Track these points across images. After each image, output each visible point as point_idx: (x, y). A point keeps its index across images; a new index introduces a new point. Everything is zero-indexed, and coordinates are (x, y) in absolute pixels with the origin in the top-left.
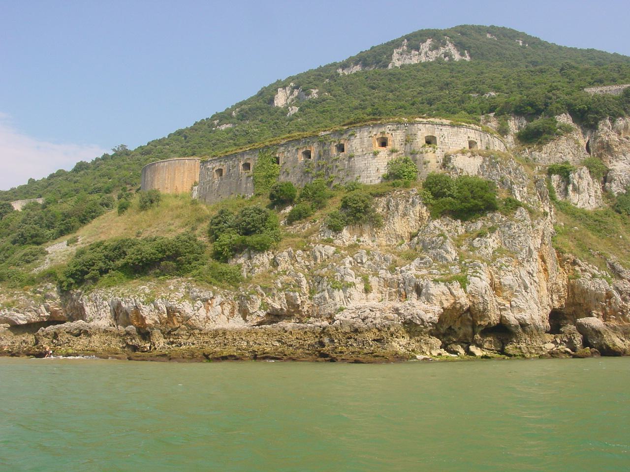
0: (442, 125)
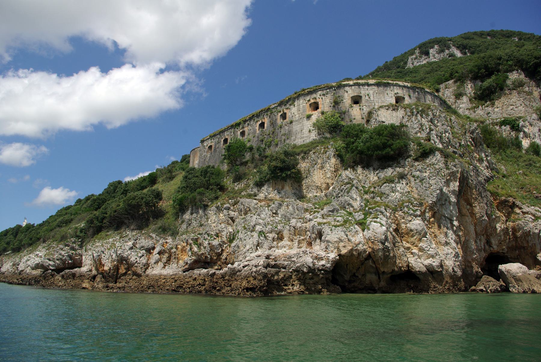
0: (368, 85)
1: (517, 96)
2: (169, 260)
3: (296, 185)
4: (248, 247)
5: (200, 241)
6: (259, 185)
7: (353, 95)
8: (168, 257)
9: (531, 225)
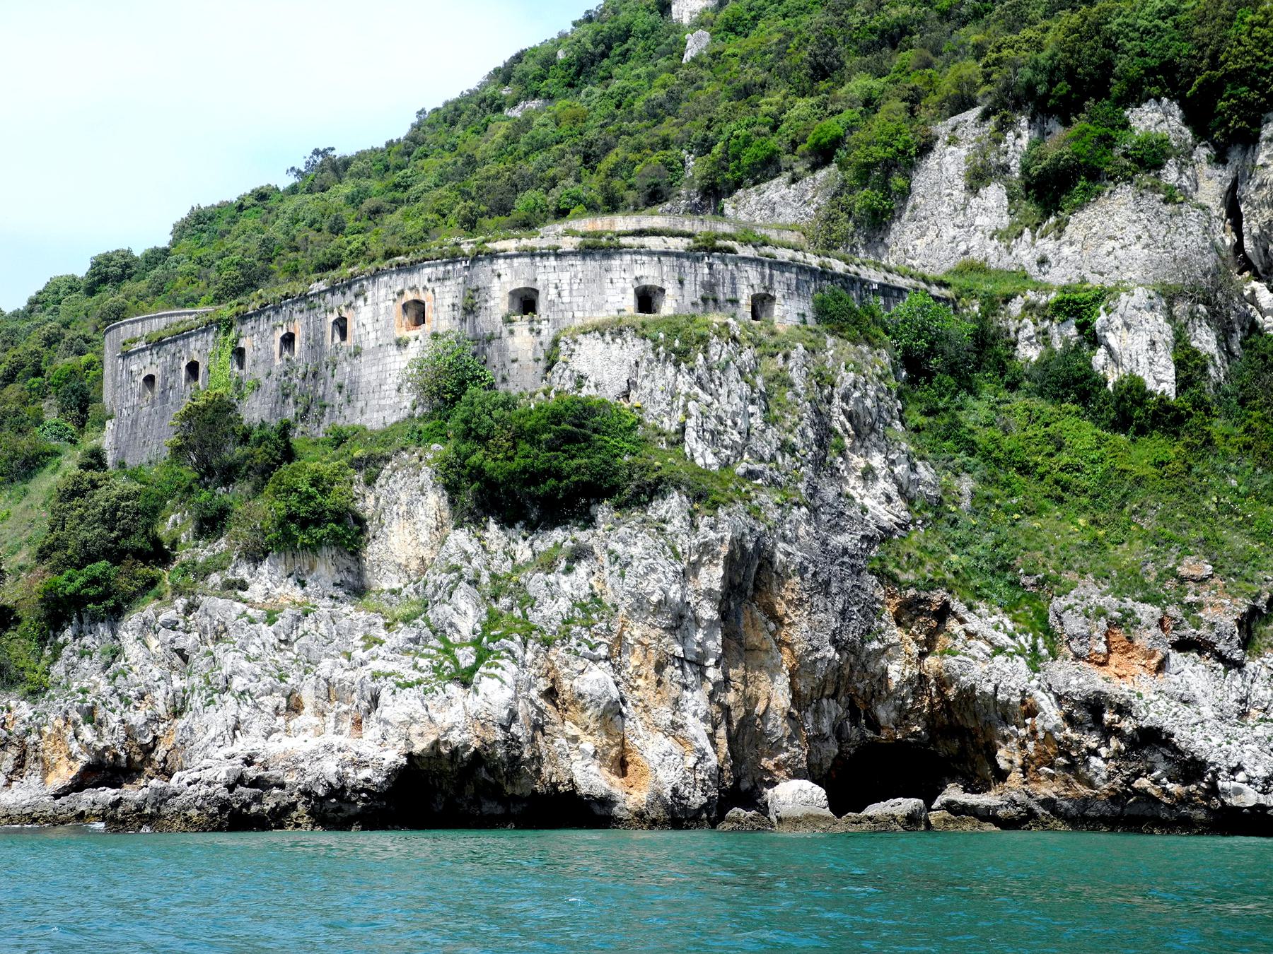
0: (558, 254)
1: (1131, 205)
2: (22, 766)
3: (348, 561)
4: (212, 733)
5: (99, 714)
6: (255, 556)
7: (515, 287)
8: (19, 757)
9: (978, 669)
